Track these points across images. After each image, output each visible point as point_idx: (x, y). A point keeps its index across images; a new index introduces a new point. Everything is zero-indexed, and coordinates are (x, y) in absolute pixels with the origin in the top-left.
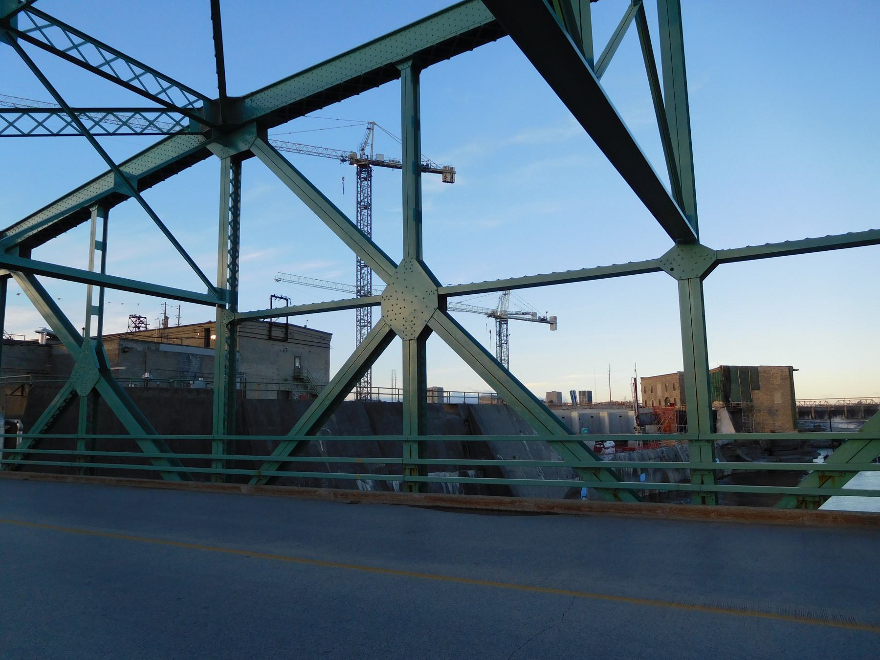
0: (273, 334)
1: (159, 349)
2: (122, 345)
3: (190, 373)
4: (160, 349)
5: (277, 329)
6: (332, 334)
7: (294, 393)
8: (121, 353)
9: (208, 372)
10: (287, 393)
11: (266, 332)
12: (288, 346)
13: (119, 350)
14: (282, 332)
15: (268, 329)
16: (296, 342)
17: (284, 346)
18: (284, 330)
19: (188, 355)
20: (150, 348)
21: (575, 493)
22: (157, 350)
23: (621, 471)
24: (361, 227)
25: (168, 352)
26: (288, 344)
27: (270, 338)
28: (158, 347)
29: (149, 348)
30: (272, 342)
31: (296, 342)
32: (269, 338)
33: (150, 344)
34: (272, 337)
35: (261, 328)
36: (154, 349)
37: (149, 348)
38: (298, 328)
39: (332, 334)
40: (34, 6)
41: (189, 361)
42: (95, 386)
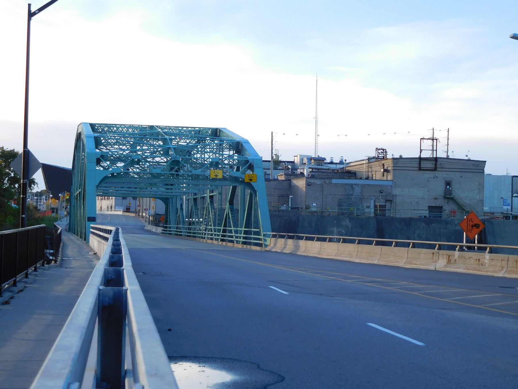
0: (422, 166)
1: (331, 182)
2: (308, 181)
3: (354, 196)
4: (332, 183)
5: (424, 162)
6: (486, 161)
7: (444, 208)
8: (307, 186)
9: (368, 195)
10: (440, 209)
11: (417, 165)
12: (436, 173)
13: (306, 184)
14: (432, 164)
15: (419, 163)
16: (447, 170)
17: (434, 174)
18: (434, 162)
19: (352, 185)
20: (326, 182)
21: (199, 209)
22: (330, 183)
23: (275, 213)
24: (139, 150)
25: (338, 184)
26: (437, 172)
27: (420, 169)
28: (331, 181)
29: (325, 182)
30: (422, 172)
31: (447, 170)
32: (419, 169)
33: (326, 180)
34: (421, 168)
35: (411, 162)
36: (328, 182)
37: (325, 182)
38: (407, 160)
39: (486, 161)
40: (40, 169)
41: (353, 189)
42: (214, 196)
